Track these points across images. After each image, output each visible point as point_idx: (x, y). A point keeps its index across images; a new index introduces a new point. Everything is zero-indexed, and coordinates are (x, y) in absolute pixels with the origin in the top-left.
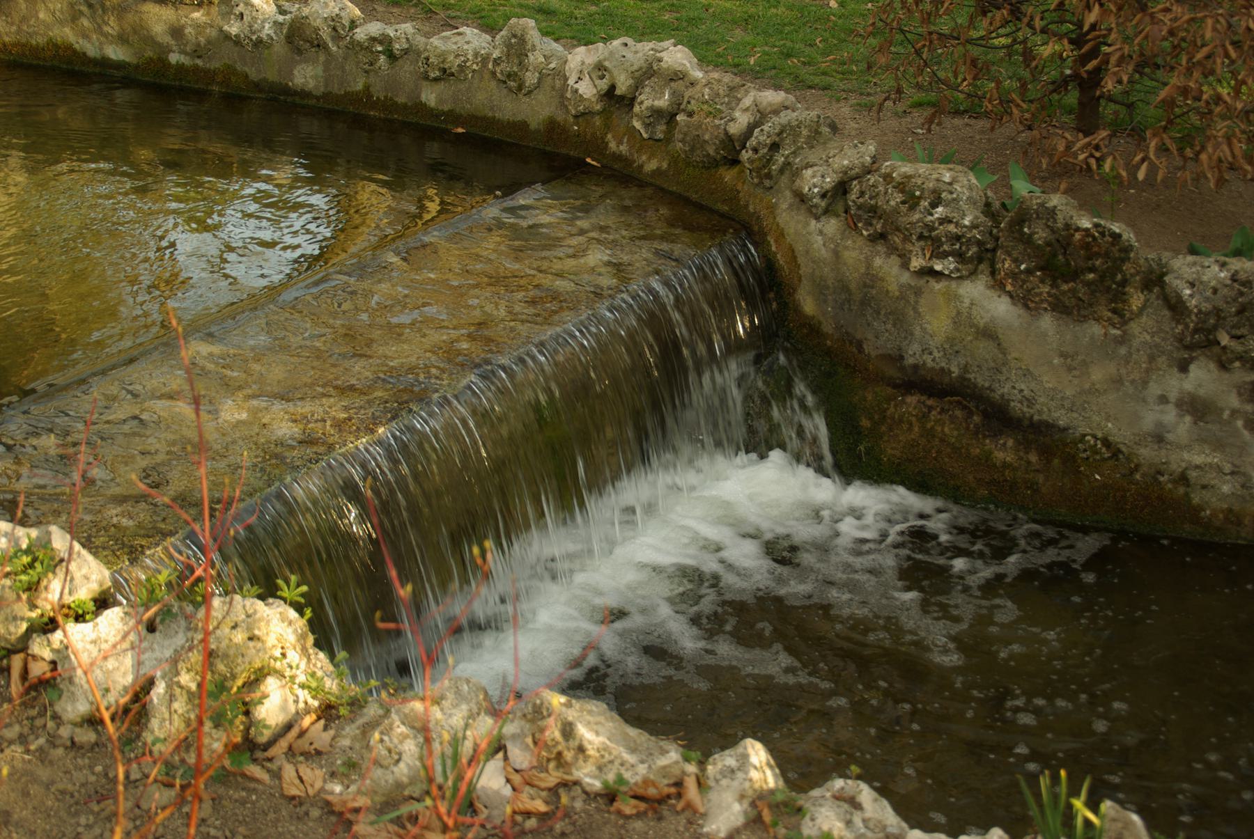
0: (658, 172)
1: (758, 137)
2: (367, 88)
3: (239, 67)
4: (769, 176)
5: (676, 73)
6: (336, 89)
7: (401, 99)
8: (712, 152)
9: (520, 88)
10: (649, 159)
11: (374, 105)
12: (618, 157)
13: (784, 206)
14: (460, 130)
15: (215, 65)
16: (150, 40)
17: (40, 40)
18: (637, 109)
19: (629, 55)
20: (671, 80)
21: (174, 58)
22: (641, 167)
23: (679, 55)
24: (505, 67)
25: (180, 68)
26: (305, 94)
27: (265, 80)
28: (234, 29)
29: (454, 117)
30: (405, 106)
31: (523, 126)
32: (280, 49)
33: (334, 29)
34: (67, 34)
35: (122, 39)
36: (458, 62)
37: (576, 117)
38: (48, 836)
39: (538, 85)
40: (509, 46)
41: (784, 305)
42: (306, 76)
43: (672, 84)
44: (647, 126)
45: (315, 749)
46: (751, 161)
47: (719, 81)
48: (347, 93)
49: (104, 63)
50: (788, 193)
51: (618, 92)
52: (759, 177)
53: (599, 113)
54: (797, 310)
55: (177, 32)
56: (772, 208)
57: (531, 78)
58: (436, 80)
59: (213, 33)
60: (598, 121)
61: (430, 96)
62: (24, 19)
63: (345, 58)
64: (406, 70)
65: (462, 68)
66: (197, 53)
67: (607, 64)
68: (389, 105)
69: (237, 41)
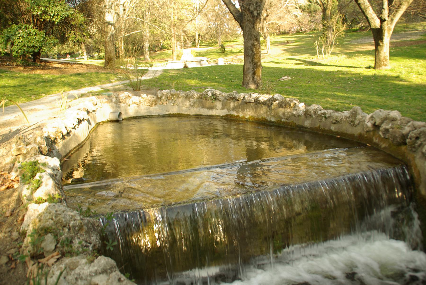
0: (385, 148)
1: (412, 134)
2: (319, 126)
3: (295, 122)
4: (414, 147)
5: (394, 118)
6: (313, 127)
7: (326, 129)
8: (399, 140)
9: (354, 125)
10: (383, 144)
11: (320, 130)
12: (375, 144)
13: (418, 157)
14: (339, 137)
15: (290, 121)
16: (279, 116)
17: (261, 117)
18: (381, 129)
19: (381, 113)
20: (393, 121)
21: (283, 120)
22: (381, 146)
23: (395, 113)
24: (351, 119)
25: (284, 122)
26: (306, 128)
27: (299, 124)
28: (294, 113)
29: (338, 133)
30: (327, 130)
31: (353, 135)
32: (303, 117)
33: (315, 112)
34: (265, 116)
35: (274, 116)
36: (340, 119)
37: (366, 132)
38: (1, 273)
39: (359, 124)
40: (352, 114)
41: (415, 191)
42: (307, 123)
43: (393, 122)
44: (384, 134)
45: (47, 264)
46: (409, 142)
47: (404, 119)
48: (315, 127)
49: (270, 122)
50: (420, 153)
51: (376, 124)
52: (411, 147)
53: (372, 131)
54: (419, 192)
55: (284, 114)
56: (414, 158)
57: (357, 122)
58: (335, 123)
59: (290, 114)
60: (371, 133)
61: (333, 128)
62: (259, 113)
63: (316, 119)
64: (329, 120)
65: (341, 120)
66: (287, 119)
67: (374, 116)
68: (324, 130)
69: (294, 116)
